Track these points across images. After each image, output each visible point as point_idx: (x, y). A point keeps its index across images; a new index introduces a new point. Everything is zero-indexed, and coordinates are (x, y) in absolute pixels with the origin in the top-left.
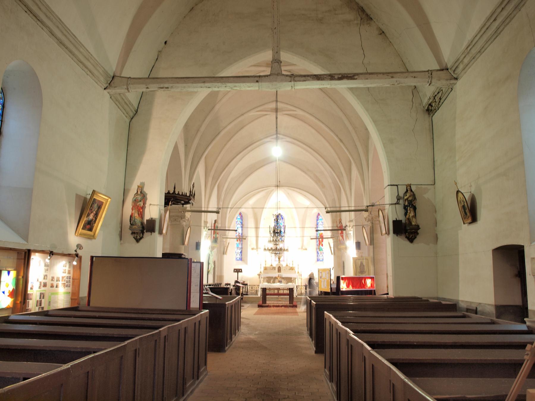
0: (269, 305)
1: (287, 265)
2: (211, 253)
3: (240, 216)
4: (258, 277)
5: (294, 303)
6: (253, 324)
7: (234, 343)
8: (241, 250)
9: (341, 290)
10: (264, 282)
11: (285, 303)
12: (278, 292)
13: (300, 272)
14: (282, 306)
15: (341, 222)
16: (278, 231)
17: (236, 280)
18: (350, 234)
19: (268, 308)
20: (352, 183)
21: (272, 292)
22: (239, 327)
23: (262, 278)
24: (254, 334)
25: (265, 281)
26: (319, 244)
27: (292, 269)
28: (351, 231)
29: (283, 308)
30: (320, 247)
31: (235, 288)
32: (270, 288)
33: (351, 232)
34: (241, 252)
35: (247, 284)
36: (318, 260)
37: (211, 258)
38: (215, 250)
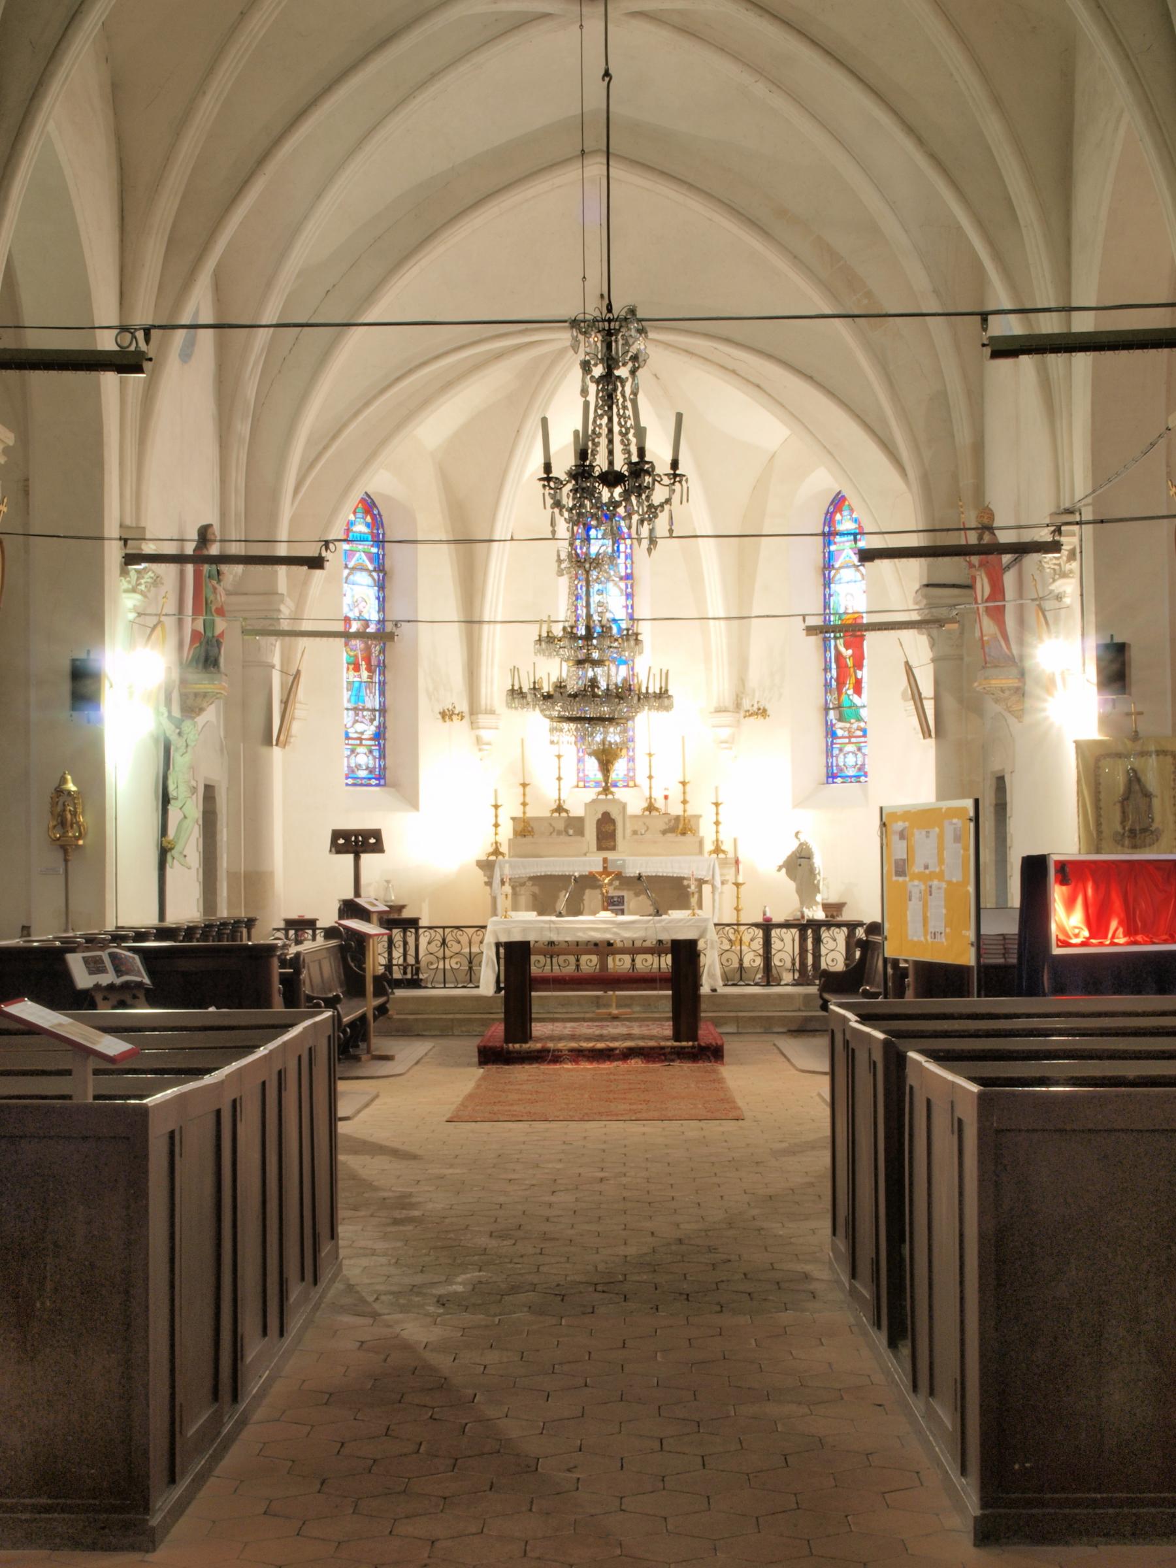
0: (551, 1045)
1: (651, 808)
2: (180, 734)
3: (369, 519)
4: (480, 876)
5: (706, 1034)
6: (435, 1202)
7: (259, 1415)
8: (376, 723)
9: (1057, 951)
10: (515, 908)
11: (644, 1031)
12: (603, 964)
13: (727, 846)
14: (629, 1054)
16: (617, 467)
17: (349, 895)
18: (1059, 598)
20: (1077, 259)
21: (565, 966)
22: (326, 1249)
23: (503, 883)
24: (441, 1302)
25: (523, 900)
26: (841, 682)
28: (1064, 575)
29: (635, 1063)
30: (844, 697)
31: (340, 947)
32: (552, 943)
33: (1069, 588)
34: (379, 736)
35: (413, 923)
36: (831, 776)
37: (180, 761)
38: (211, 715)
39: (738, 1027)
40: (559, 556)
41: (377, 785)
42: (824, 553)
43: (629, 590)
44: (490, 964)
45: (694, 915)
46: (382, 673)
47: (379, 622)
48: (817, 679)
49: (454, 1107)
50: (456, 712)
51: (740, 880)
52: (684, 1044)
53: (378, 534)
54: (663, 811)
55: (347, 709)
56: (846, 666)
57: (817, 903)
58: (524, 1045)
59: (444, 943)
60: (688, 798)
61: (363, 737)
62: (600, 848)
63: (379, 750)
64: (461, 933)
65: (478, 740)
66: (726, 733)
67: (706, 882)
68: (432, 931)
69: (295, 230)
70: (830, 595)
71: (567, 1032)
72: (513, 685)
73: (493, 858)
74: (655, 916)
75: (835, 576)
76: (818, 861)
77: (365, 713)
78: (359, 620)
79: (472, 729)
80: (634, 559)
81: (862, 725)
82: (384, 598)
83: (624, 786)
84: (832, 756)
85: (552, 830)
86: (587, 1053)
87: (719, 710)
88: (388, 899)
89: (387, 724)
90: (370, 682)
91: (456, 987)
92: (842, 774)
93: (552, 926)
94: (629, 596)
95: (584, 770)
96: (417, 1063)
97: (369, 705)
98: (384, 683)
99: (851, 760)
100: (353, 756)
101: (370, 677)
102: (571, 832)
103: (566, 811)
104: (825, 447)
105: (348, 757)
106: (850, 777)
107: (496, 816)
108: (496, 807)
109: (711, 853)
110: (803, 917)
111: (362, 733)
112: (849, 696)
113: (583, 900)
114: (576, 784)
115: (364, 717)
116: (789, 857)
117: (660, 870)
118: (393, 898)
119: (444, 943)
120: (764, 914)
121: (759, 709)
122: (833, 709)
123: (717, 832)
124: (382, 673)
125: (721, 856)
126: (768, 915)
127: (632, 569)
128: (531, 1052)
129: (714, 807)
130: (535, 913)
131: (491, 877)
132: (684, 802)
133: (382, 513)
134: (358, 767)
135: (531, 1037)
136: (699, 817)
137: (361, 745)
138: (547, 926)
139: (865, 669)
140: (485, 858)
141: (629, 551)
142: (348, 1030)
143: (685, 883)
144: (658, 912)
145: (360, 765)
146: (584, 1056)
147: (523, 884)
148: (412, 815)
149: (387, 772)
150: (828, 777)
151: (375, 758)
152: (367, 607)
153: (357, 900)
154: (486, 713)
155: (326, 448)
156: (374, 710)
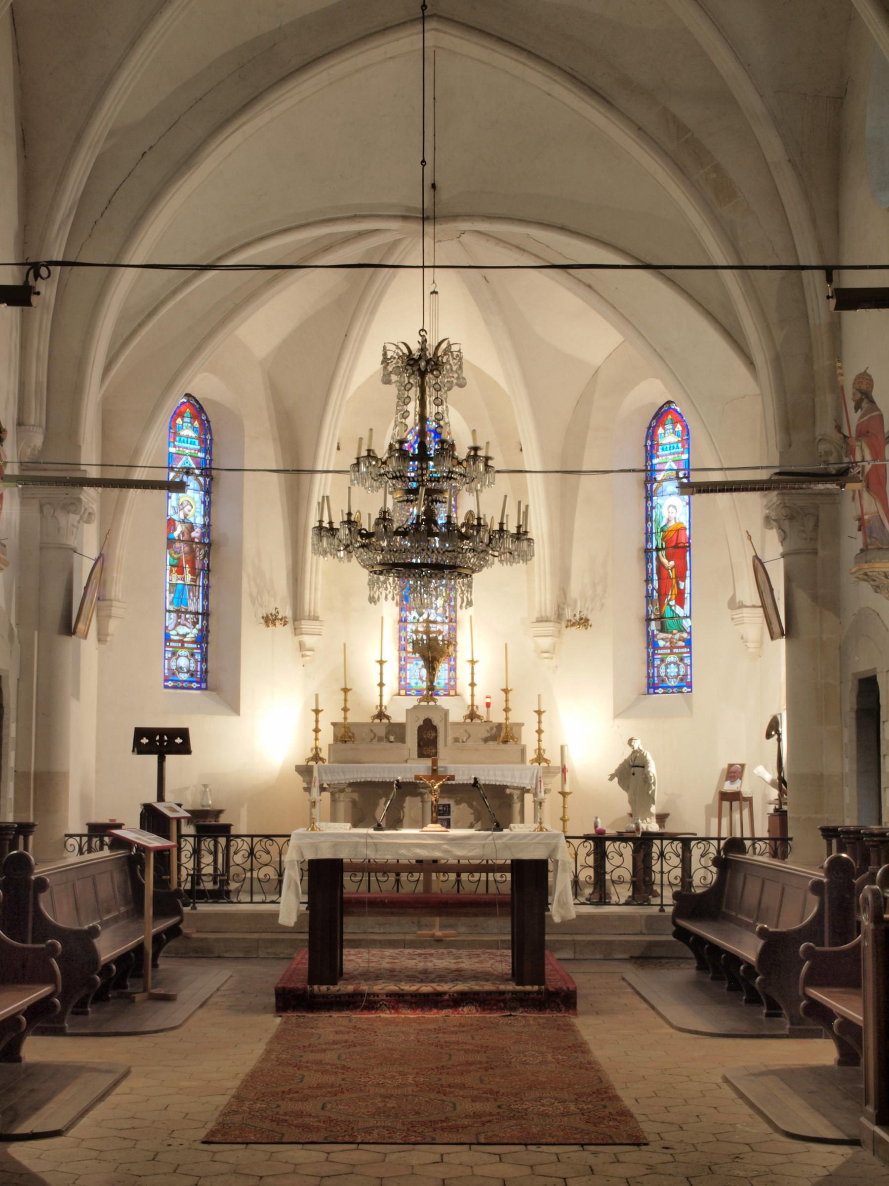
0: (365, 987)
1: (472, 716)
3: (196, 424)
4: (299, 781)
8: (199, 626)
12: (428, 882)
14: (459, 1000)
15: (872, 401)
19: (357, 1016)
21: (384, 886)
26: (662, 594)
29: (469, 1013)
30: (666, 609)
34: (203, 639)
36: (653, 686)
39: (575, 953)
40: (385, 354)
41: (197, 689)
44: (293, 887)
45: (541, 830)
46: (207, 576)
47: (204, 525)
49: (222, 1101)
50: (280, 617)
51: (567, 789)
52: (528, 988)
53: (206, 440)
54: (485, 719)
55: (170, 611)
56: (669, 577)
57: (651, 815)
58: (332, 987)
59: (252, 853)
60: (510, 706)
61: (186, 640)
62: (421, 755)
63: (201, 653)
64: (270, 842)
65: (302, 646)
66: (546, 642)
67: (528, 791)
69: (108, 82)
70: (652, 508)
71: (385, 964)
72: (321, 521)
73: (312, 763)
74: (495, 830)
75: (657, 488)
76: (652, 769)
77: (188, 616)
78: (184, 522)
79: (296, 635)
81: (685, 635)
82: (210, 502)
83: (445, 695)
84: (653, 667)
85: (373, 736)
86: (409, 998)
87: (541, 620)
88: (205, 803)
89: (210, 628)
90: (194, 585)
91: (263, 902)
92: (664, 685)
93: (369, 840)
95: (406, 678)
96: (201, 1006)
97: (192, 608)
98: (208, 587)
99: (673, 670)
100: (174, 659)
101: (194, 580)
102: (392, 738)
103: (388, 717)
104: (655, 351)
105: (169, 659)
107: (317, 721)
108: (317, 711)
109: (533, 761)
110: (638, 829)
111: (184, 636)
112: (671, 606)
113: (403, 808)
114: (397, 692)
115: (186, 619)
116: (620, 765)
118: (210, 803)
119: (252, 853)
120: (596, 827)
121: (581, 619)
122: (655, 620)
123: (539, 740)
124: (207, 576)
125: (544, 764)
126: (600, 826)
128: (340, 996)
129: (536, 715)
130: (349, 825)
131: (309, 783)
132: (507, 710)
134: (180, 669)
135: (341, 973)
136: (523, 724)
137: (183, 647)
138: (363, 840)
139: (688, 581)
140: (304, 763)
142: (114, 967)
143: (508, 791)
144: (498, 825)
145: (181, 668)
146: (405, 1002)
147: (342, 791)
148: (233, 719)
149: (209, 675)
150: (649, 687)
151: (196, 661)
152: (193, 510)
153: (160, 807)
154: (309, 619)
155: (141, 325)
156: (197, 613)
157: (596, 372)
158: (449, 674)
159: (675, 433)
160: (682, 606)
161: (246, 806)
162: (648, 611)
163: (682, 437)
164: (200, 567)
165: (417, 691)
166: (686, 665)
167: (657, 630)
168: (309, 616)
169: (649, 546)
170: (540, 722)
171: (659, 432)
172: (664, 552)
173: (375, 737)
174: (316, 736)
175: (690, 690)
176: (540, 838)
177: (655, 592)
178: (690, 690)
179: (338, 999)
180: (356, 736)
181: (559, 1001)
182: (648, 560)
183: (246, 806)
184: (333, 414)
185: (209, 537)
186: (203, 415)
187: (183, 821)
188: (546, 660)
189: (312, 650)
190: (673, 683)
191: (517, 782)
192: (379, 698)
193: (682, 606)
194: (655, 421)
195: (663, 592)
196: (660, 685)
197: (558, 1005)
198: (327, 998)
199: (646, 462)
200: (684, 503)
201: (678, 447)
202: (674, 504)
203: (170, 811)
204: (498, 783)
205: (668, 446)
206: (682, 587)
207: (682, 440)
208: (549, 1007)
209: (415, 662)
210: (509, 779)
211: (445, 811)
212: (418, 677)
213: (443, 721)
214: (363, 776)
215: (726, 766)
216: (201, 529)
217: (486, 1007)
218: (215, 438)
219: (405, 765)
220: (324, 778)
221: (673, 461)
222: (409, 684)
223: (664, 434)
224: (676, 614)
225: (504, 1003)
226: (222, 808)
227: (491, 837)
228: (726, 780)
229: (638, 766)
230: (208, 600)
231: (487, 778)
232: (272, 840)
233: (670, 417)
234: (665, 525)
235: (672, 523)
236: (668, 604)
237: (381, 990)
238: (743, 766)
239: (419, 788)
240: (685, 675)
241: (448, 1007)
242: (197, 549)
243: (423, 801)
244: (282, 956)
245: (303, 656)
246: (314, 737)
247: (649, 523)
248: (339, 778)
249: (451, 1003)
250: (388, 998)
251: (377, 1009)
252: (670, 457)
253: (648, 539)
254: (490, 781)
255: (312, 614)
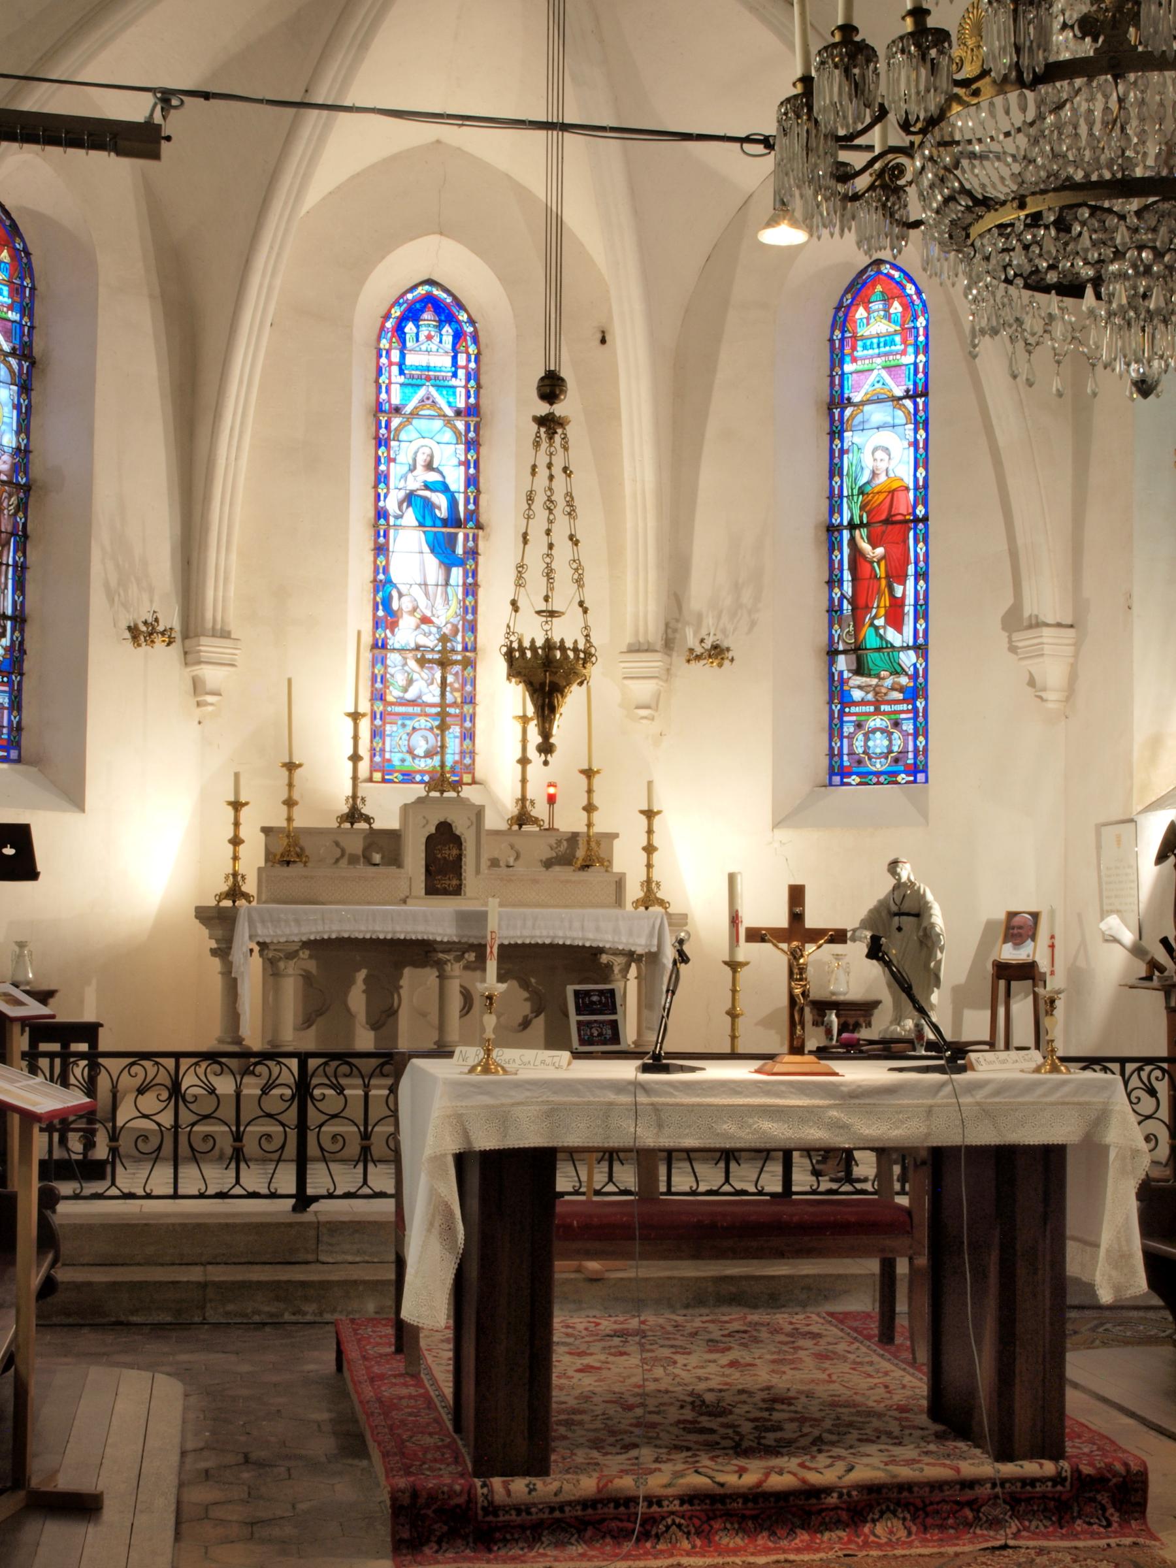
4: (203, 938)
26: (860, 607)
27: (581, 853)
42: (832, 377)
43: (472, 435)
47: (18, 449)
48: (815, 599)
50: (161, 628)
52: (1030, 1468)
56: (874, 576)
58: (538, 1482)
65: (197, 686)
66: (644, 689)
68: (147, 1064)
70: (842, 452)
75: (852, 417)
76: (938, 918)
80: (483, 381)
82: (29, 407)
84: (841, 737)
85: (338, 852)
86: (737, 1505)
87: (636, 649)
89: (27, 645)
92: (862, 769)
93: (642, 1099)
94: (472, 445)
95: (383, 750)
98: (24, 567)
102: (377, 858)
103: (368, 819)
106: (878, 774)
107: (237, 824)
108: (237, 805)
109: (637, 904)
112: (877, 628)
113: (398, 988)
116: (871, 911)
117: (560, 934)
122: (844, 652)
127: (477, 396)
129: (643, 820)
132: (590, 808)
133: (31, 249)
136: (616, 836)
138: (625, 1099)
140: (213, 903)
141: (472, 365)
143: (604, 958)
146: (729, 1515)
148: (71, 818)
149: (24, 734)
150: (832, 772)
154: (213, 636)
157: (746, 202)
158: (461, 745)
159: (888, 317)
160: (899, 630)
161: (94, 982)
162: (831, 636)
163: (902, 326)
164: (9, 529)
165: (403, 775)
166: (906, 734)
167: (849, 671)
168: (214, 628)
169: (836, 520)
170: (650, 832)
171: (858, 316)
172: (864, 531)
173: (343, 855)
174: (235, 852)
175: (912, 778)
176: (1066, 1089)
177: (845, 602)
178: (912, 778)
179: (557, 1514)
180: (307, 852)
181: (1103, 1498)
182: (833, 546)
183: (94, 982)
184: (271, 248)
185: (26, 474)
186: (18, 240)
187: (796, 1154)
188: (644, 721)
189: (217, 693)
190: (878, 766)
191: (623, 941)
192: (350, 782)
193: (899, 630)
194: (849, 296)
195: (861, 602)
196: (855, 769)
197: (1104, 1509)
198: (529, 1513)
199: (832, 370)
200: (906, 444)
201: (893, 343)
202: (886, 445)
203: (7, 1002)
204: (588, 944)
205: (875, 341)
206: (899, 594)
207: (903, 329)
208: (1079, 1517)
209: (400, 722)
210: (609, 937)
211: (605, 1005)
212: (405, 749)
213: (474, 828)
214: (335, 927)
215: (1002, 916)
216: (12, 456)
217: (929, 1521)
218: (41, 287)
219: (404, 908)
220: (259, 932)
221: (884, 368)
222: (389, 760)
223: (868, 319)
224: (887, 642)
225: (972, 1510)
226: (52, 988)
227: (949, 1088)
228: (1005, 941)
229: (908, 914)
230: (23, 593)
231: (568, 934)
232: (220, 1063)
233: (879, 288)
234: (868, 483)
235: (882, 478)
236: (872, 625)
237: (666, 1486)
238: (1035, 916)
239: (435, 951)
240: (904, 752)
241: (838, 1524)
242: (5, 495)
243: (442, 977)
244: (257, 1318)
245: (199, 704)
246: (231, 854)
247: (837, 479)
248: (287, 931)
249: (844, 1516)
250: (686, 1507)
251: (658, 1537)
252: (878, 361)
253: (834, 506)
254: (574, 939)
255: (219, 627)
